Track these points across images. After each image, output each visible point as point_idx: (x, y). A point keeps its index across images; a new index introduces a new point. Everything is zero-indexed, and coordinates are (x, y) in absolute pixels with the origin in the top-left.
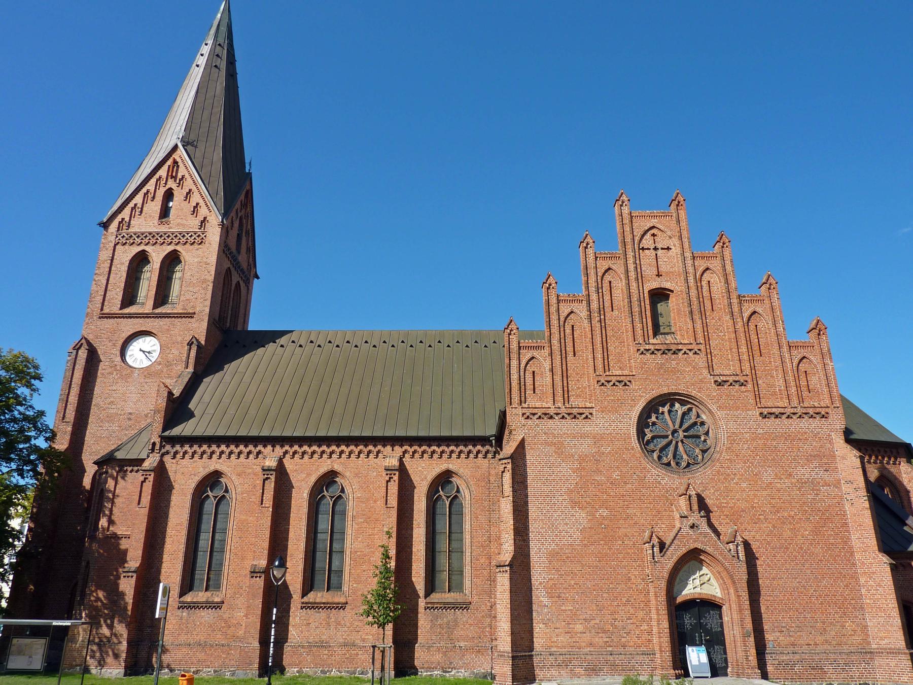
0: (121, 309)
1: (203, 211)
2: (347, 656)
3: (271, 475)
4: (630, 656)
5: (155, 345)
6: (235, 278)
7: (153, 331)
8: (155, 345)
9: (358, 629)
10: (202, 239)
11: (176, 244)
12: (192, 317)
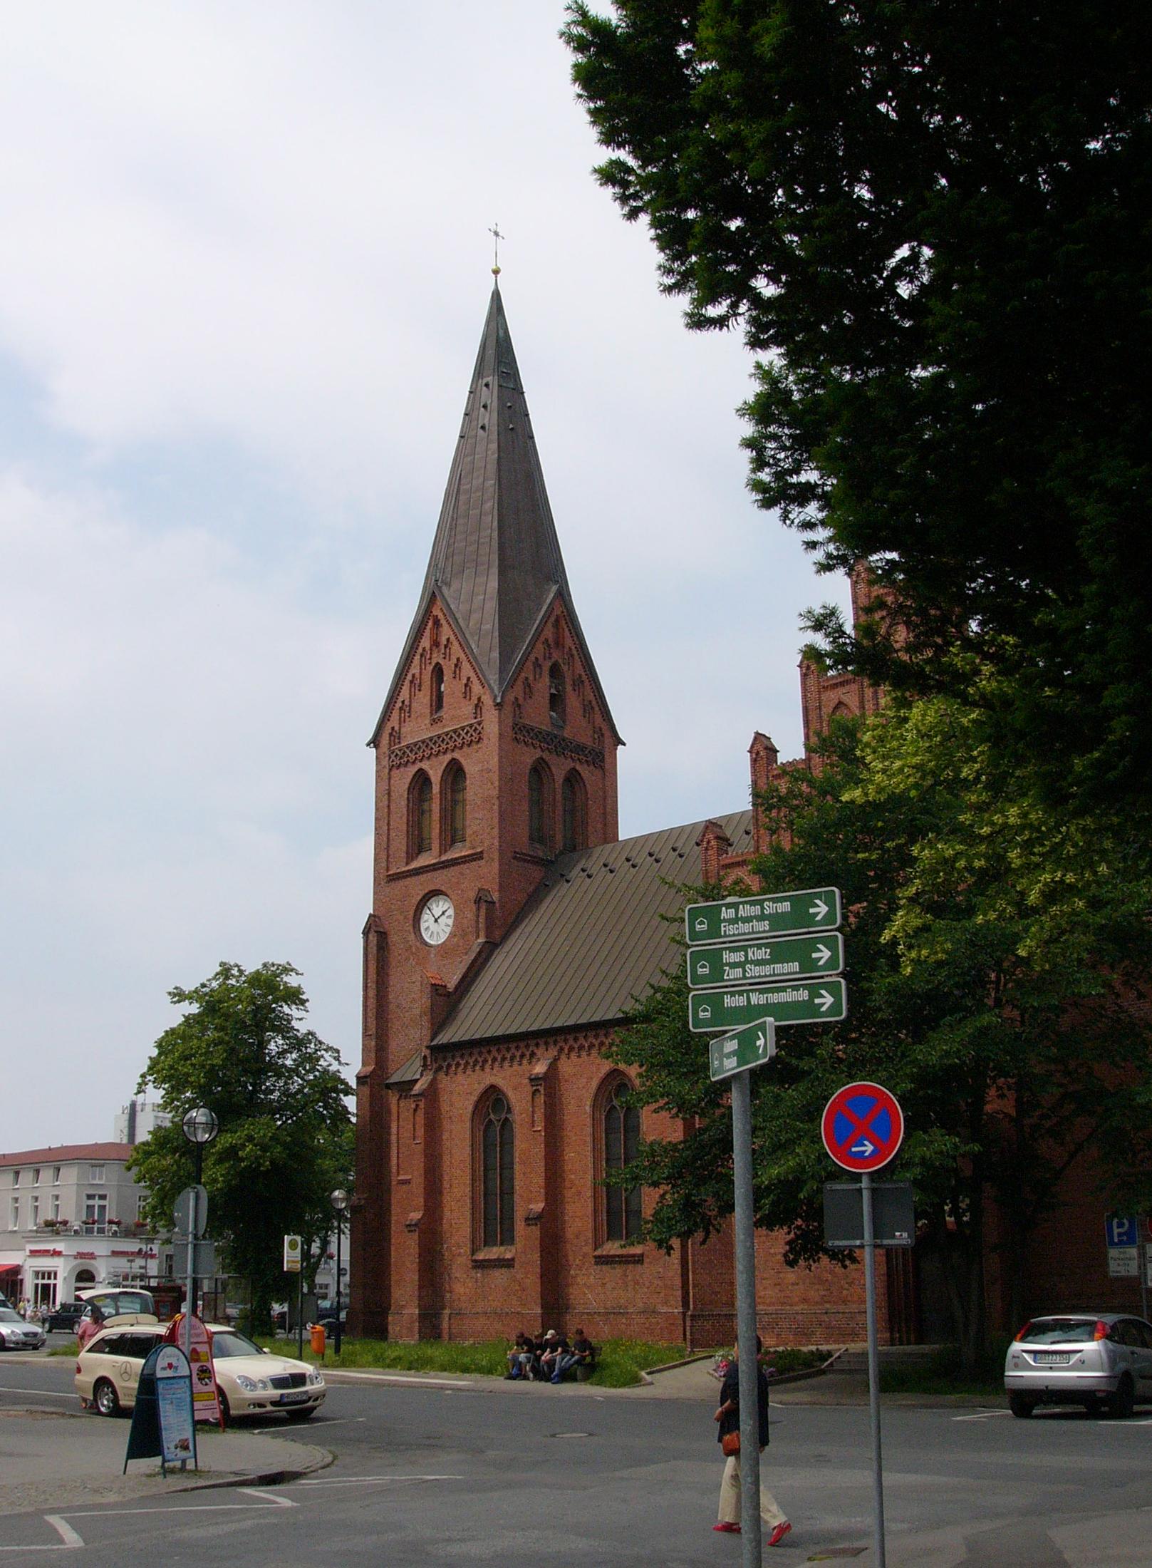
0: (407, 864)
2: (647, 1325)
3: (541, 1085)
4: (849, 1316)
6: (560, 768)
7: (443, 888)
9: (658, 1290)
10: (480, 733)
11: (453, 751)
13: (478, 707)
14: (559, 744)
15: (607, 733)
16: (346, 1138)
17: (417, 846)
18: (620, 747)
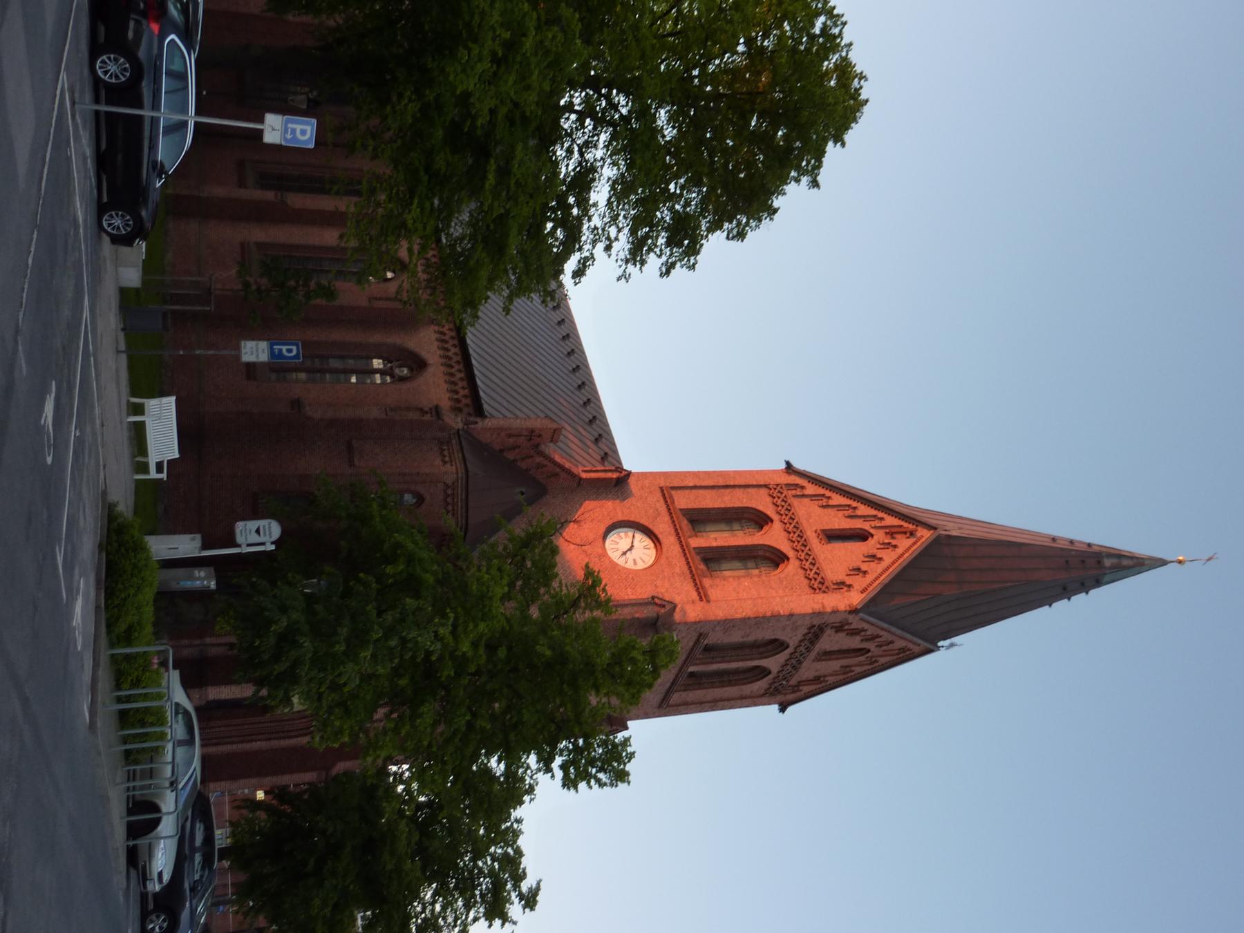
1: (859, 582)
5: (644, 562)
6: (773, 663)
8: (644, 562)
12: (701, 599)
13: (841, 585)
14: (795, 663)
15: (791, 697)
16: (713, 79)
17: (699, 519)
18: (776, 707)
